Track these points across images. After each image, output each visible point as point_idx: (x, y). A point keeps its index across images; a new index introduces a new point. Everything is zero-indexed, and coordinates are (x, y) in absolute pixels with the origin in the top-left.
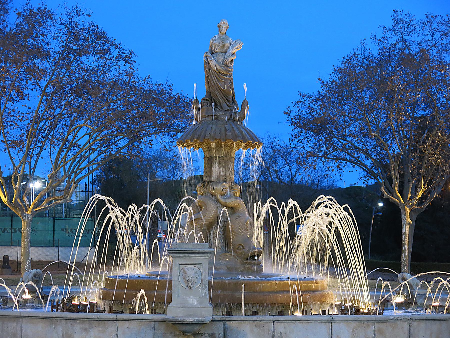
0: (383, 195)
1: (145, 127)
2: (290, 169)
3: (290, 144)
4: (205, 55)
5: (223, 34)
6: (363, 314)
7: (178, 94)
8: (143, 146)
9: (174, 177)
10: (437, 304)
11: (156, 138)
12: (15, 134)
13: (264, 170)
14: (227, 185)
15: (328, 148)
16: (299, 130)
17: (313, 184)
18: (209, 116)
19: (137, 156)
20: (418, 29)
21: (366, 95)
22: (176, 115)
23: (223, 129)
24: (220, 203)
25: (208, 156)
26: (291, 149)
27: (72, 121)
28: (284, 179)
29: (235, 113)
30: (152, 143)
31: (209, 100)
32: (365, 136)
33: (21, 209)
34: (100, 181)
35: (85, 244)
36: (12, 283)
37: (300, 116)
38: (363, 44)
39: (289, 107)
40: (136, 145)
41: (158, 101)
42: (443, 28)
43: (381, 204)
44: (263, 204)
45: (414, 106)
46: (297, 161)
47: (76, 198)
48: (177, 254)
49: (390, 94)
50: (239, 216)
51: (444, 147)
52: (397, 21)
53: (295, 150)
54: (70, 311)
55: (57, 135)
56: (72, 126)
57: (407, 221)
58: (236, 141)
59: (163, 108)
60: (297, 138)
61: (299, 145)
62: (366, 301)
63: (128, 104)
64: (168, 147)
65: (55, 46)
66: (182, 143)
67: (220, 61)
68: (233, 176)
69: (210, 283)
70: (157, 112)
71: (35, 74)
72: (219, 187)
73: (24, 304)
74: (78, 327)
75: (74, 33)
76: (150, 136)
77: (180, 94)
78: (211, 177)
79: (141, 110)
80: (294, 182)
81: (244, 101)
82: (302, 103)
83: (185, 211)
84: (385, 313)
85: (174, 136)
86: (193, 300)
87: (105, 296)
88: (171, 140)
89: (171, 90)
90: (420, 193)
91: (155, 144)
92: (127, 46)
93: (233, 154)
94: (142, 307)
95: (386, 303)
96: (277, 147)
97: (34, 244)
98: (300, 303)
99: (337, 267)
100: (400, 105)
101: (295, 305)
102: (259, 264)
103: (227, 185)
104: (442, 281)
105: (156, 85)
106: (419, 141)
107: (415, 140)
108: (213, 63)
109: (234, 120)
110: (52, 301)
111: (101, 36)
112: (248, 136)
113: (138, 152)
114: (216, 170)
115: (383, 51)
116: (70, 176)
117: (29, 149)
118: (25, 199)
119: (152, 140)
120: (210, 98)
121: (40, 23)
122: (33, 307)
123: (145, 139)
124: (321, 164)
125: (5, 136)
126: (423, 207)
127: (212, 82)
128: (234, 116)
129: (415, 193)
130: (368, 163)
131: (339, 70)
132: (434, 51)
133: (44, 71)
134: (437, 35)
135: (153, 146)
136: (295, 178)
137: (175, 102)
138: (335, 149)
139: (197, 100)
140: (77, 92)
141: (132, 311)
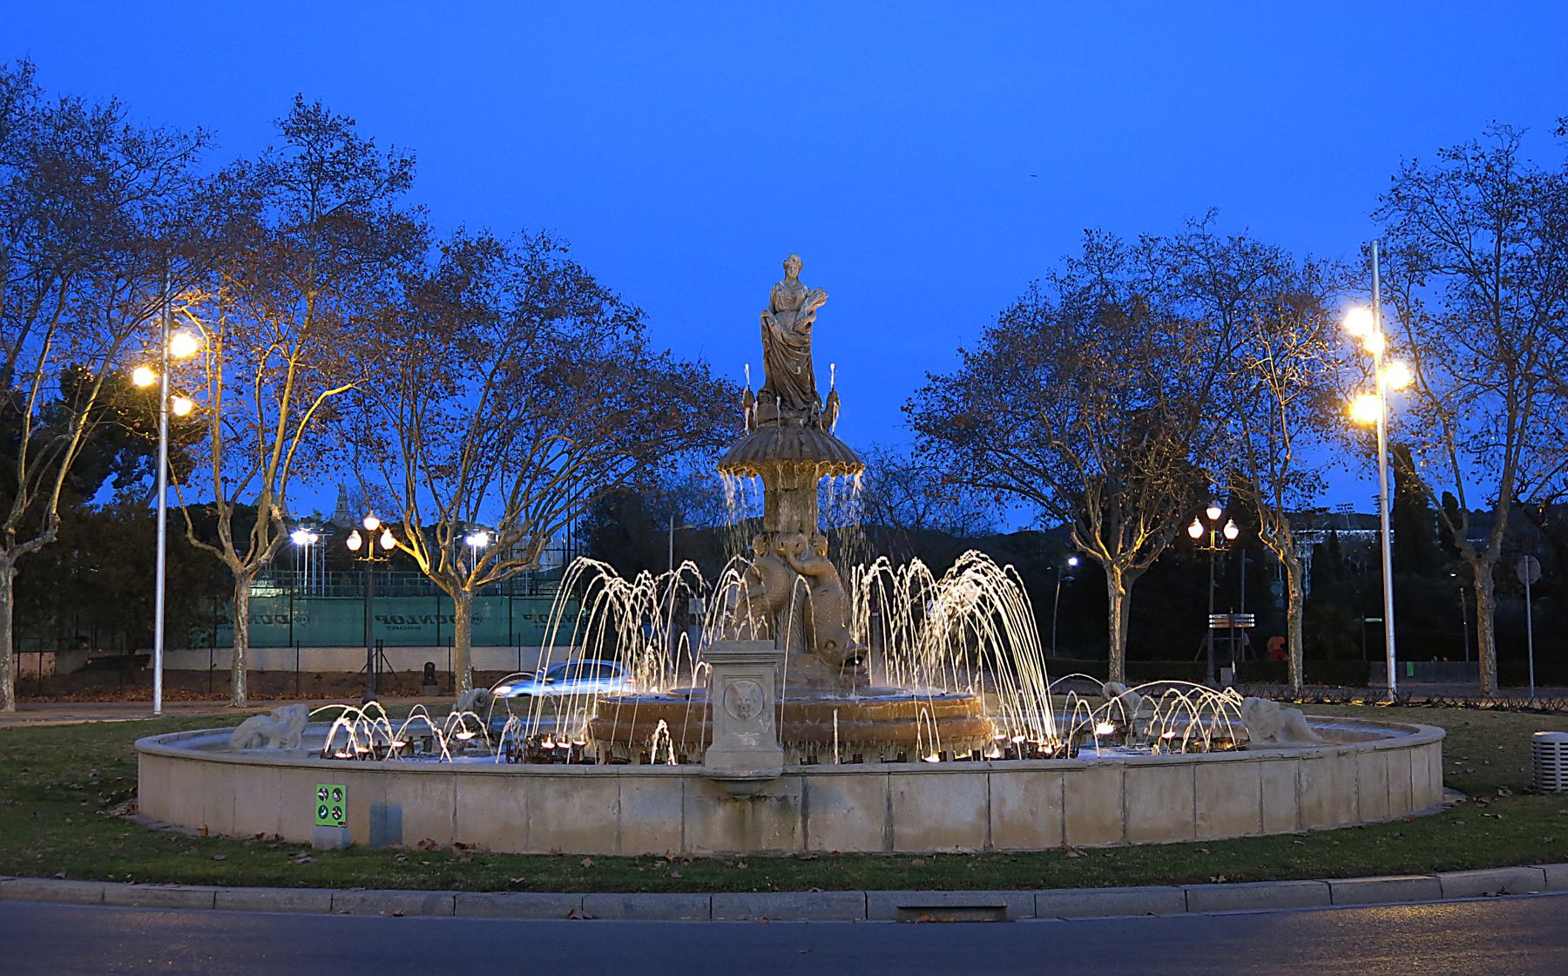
0: (1075, 546)
2: (915, 505)
6: (1048, 757)
10: (1170, 735)
12: (441, 454)
14: (805, 538)
15: (978, 468)
17: (953, 529)
20: (1127, 260)
21: (1042, 374)
27: (538, 431)
32: (1040, 445)
33: (454, 584)
34: (587, 531)
35: (563, 641)
36: (439, 713)
38: (1033, 288)
42: (1170, 259)
43: (1073, 562)
45: (1123, 393)
47: (547, 562)
48: (720, 659)
49: (1082, 374)
51: (1176, 463)
52: (1092, 248)
54: (538, 760)
55: (513, 455)
56: (538, 439)
57: (1117, 589)
61: (928, 463)
62: (1048, 732)
63: (635, 400)
64: (703, 472)
65: (507, 303)
69: (778, 707)
71: (473, 350)
72: (791, 542)
73: (459, 748)
74: (551, 790)
75: (539, 280)
83: (733, 579)
84: (1082, 753)
86: (749, 740)
87: (597, 733)
90: (1139, 542)
91: (681, 467)
92: (630, 301)
94: (662, 750)
95: (1084, 733)
97: (476, 642)
98: (934, 739)
99: (996, 672)
100: (1101, 393)
101: (925, 741)
102: (862, 673)
103: (805, 538)
106: (1134, 453)
107: (1127, 451)
108: (776, 329)
109: (814, 425)
110: (508, 743)
111: (587, 285)
114: (784, 509)
115: (1069, 300)
116: (537, 524)
117: (465, 482)
118: (460, 565)
120: (773, 389)
121: (481, 264)
122: (472, 754)
124: (967, 496)
125: (424, 459)
126: (1145, 565)
129: (1131, 543)
130: (1048, 491)
131: (995, 334)
132: (1156, 299)
133: (489, 345)
134: (1161, 271)
138: (991, 469)
140: (546, 381)
141: (645, 760)
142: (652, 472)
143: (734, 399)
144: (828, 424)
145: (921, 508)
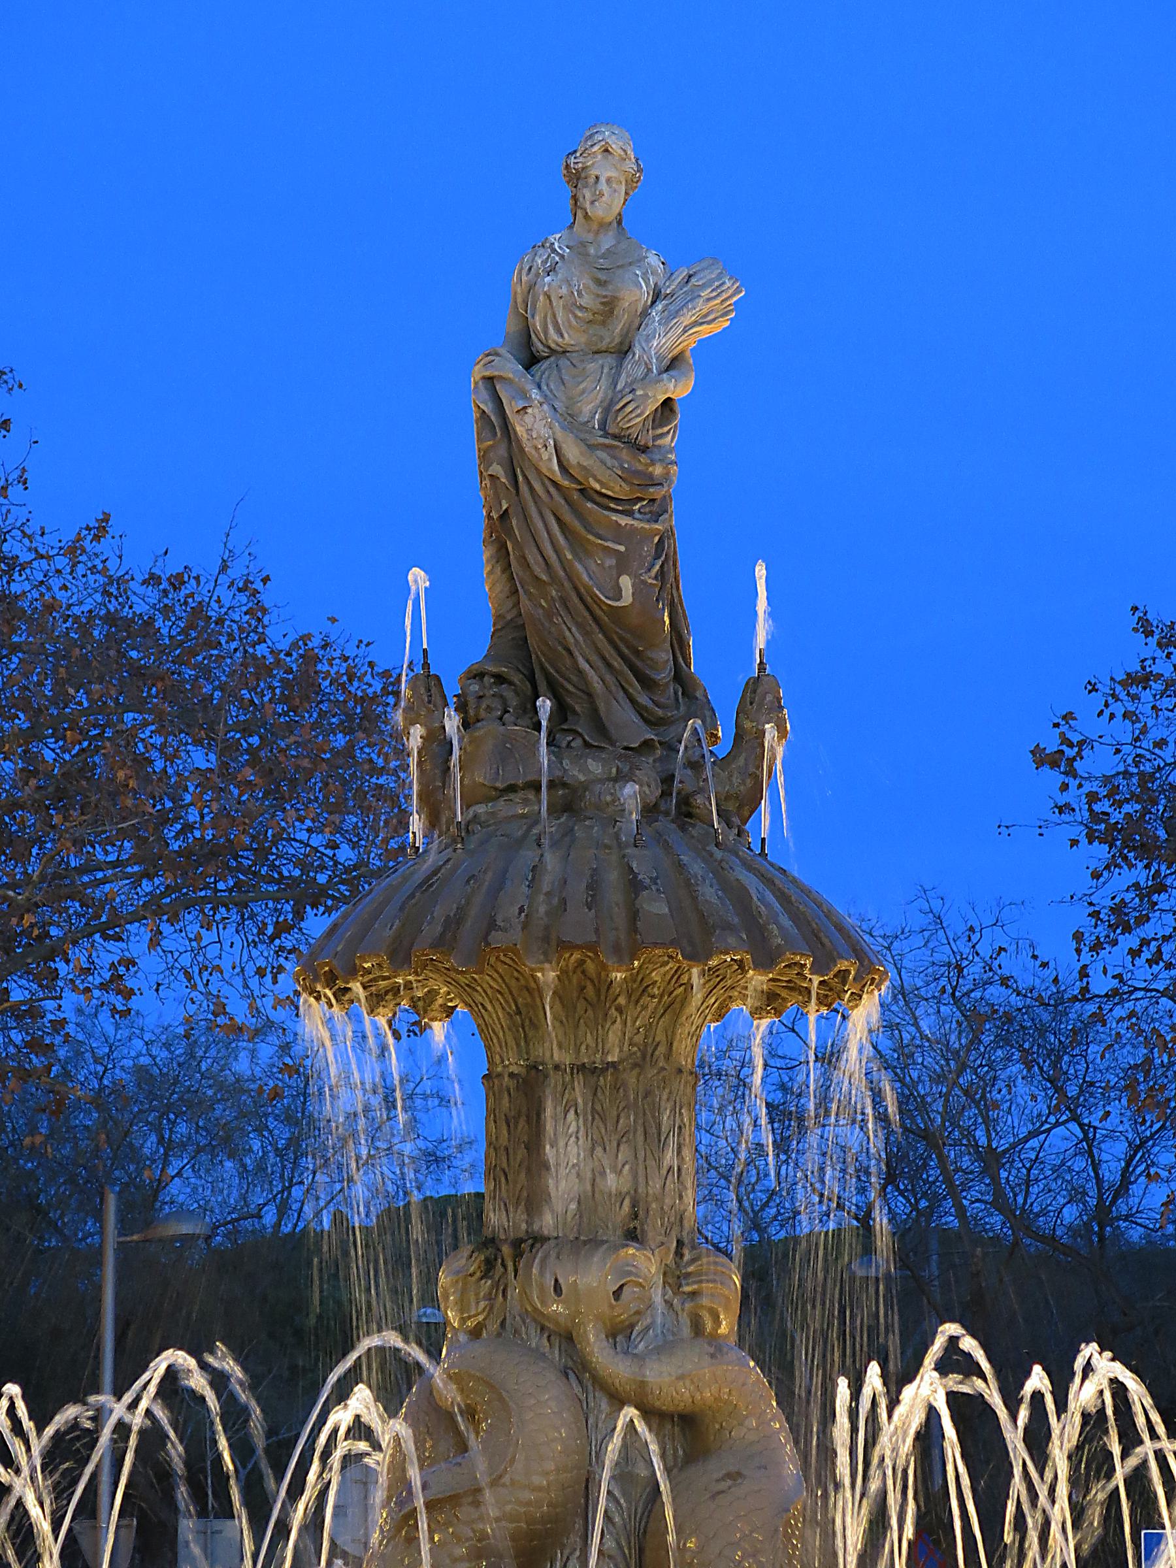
1: (81, 870)
2: (1088, 1144)
3: (1084, 973)
4: (478, 372)
5: (603, 226)
7: (305, 638)
8: (70, 999)
9: (283, 1210)
11: (154, 943)
13: (914, 1152)
14: (648, 1264)
16: (1139, 874)
18: (512, 788)
19: (25, 1075)
22: (293, 782)
23: (613, 876)
24: (600, 1383)
25: (515, 1063)
26: (1091, 1008)
28: (1044, 1212)
29: (695, 766)
30: (130, 983)
31: (516, 678)
37: (1145, 779)
39: (1068, 717)
40: (17, 996)
41: (164, 695)
44: (896, 1381)
46: (1131, 1087)
50: (735, 1476)
53: (1119, 1012)
58: (694, 957)
59: (207, 742)
60: (1127, 929)
61: (1142, 974)
64: (239, 1010)
66: (331, 980)
67: (587, 409)
68: (689, 1196)
70: (159, 765)
72: (593, 1277)
76: (112, 930)
77: (315, 642)
78: (534, 1201)
79: (49, 755)
80: (1119, 1234)
81: (753, 685)
82: (1157, 686)
85: (282, 929)
88: (263, 956)
89: (258, 611)
93: (683, 1046)
96: (995, 993)
103: (648, 1264)
104: (1164, 1528)
105: (152, 580)
108: (535, 426)
109: (686, 812)
112: (785, 921)
113: (35, 1045)
114: (573, 1160)
119: (130, 963)
120: (522, 671)
123: (79, 956)
127: (532, 557)
128: (689, 787)
135: (135, 1003)
136: (1122, 1207)
137: (284, 699)
139: (429, 683)
142: (33, 1011)
143: (365, 717)
144: (748, 802)
145: (1112, 1155)
